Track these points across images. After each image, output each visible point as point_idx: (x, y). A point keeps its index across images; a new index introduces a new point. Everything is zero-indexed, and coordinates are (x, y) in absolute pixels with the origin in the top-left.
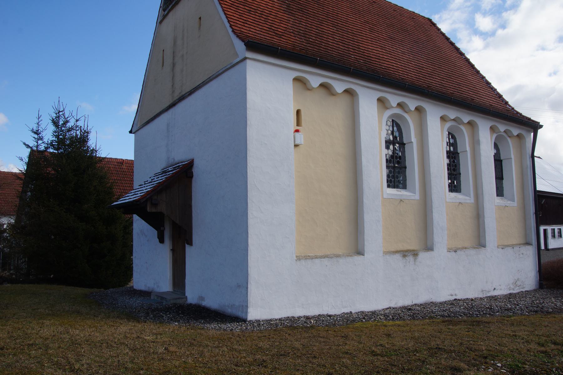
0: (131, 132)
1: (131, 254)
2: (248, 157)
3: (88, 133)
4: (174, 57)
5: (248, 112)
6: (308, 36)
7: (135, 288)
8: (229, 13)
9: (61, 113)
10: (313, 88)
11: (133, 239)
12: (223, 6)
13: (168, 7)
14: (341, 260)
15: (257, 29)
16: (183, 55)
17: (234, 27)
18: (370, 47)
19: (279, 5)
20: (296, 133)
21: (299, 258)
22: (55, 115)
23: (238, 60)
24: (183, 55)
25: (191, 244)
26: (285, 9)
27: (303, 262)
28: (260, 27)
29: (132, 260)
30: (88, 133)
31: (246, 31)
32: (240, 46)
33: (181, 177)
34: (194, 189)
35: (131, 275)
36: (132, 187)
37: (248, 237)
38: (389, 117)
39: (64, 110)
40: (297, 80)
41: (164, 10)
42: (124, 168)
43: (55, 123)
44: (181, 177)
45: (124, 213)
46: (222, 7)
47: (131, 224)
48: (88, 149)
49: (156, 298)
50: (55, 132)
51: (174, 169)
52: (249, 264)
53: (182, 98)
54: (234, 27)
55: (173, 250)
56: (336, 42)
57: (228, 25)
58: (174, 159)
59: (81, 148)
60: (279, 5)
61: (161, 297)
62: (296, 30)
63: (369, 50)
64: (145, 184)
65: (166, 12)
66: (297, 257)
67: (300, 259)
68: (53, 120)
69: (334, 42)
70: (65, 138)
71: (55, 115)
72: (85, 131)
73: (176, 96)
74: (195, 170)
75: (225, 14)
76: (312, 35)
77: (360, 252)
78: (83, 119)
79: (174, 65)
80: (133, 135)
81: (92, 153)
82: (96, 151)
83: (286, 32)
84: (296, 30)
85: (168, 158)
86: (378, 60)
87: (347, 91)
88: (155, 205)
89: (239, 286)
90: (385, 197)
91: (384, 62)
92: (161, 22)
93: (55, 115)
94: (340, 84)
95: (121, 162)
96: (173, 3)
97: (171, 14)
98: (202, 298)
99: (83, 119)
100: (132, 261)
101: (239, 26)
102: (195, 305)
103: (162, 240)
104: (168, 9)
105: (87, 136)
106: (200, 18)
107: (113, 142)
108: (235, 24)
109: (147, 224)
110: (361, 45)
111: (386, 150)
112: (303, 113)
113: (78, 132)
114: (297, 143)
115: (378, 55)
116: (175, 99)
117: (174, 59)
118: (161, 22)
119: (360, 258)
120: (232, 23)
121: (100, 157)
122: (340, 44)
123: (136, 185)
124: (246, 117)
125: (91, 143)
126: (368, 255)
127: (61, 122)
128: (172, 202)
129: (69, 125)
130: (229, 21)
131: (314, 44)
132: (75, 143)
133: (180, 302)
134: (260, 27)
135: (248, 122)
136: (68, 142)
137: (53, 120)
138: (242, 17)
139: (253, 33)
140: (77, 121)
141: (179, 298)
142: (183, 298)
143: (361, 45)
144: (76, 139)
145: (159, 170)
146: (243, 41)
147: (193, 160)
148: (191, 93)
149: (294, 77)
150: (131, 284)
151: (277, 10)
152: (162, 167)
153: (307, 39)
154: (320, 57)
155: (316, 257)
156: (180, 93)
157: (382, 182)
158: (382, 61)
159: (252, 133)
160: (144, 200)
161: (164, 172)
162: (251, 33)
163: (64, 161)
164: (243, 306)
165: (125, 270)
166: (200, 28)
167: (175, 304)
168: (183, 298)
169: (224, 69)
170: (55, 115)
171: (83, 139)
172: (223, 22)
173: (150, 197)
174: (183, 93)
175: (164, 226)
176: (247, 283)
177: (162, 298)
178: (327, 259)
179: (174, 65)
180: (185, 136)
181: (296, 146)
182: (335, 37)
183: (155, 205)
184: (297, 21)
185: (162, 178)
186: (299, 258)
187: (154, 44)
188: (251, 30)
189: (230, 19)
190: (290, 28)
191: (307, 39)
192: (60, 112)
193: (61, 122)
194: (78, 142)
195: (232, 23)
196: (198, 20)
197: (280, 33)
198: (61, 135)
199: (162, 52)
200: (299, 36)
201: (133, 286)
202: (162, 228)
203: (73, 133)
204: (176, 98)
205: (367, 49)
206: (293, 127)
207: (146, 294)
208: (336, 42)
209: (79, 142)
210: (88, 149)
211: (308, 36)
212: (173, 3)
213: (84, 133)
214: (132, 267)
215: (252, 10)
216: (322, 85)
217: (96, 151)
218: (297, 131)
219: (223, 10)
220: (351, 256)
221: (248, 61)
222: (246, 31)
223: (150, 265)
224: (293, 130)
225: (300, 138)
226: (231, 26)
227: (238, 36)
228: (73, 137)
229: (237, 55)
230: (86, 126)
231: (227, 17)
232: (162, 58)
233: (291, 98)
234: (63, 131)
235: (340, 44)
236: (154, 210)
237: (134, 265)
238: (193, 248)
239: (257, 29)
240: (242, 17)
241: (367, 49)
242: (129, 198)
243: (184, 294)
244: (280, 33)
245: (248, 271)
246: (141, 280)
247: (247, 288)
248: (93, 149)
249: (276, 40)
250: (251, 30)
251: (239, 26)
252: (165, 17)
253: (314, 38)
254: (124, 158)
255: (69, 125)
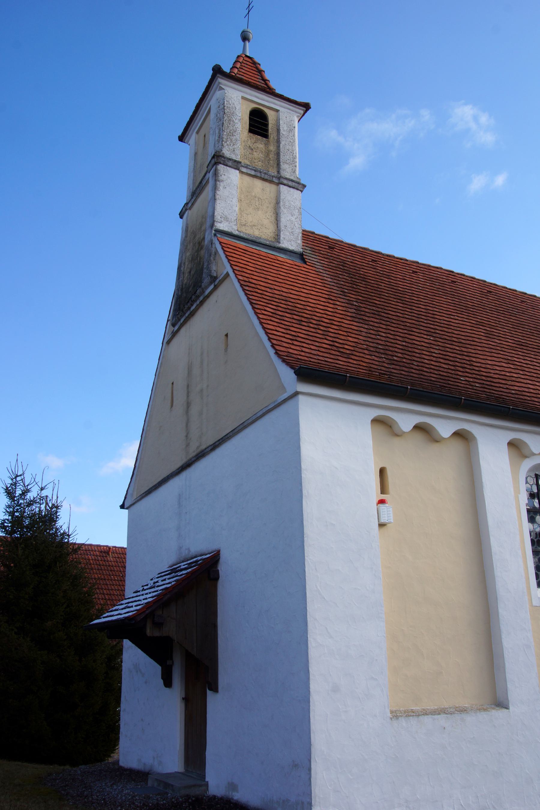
0: (122, 507)
1: (118, 702)
2: (306, 547)
3: (57, 507)
4: (188, 393)
5: (303, 475)
6: (390, 353)
7: (121, 764)
8: (269, 327)
9: (19, 479)
10: (404, 433)
11: (121, 678)
12: (261, 316)
13: (179, 320)
14: (470, 719)
15: (313, 347)
16: (202, 390)
17: (277, 347)
18: (490, 362)
19: (344, 309)
20: (381, 505)
21: (395, 715)
22: (10, 482)
23: (285, 396)
24: (202, 390)
25: (215, 689)
26: (354, 315)
27: (403, 722)
28: (317, 344)
29: (118, 714)
30: (57, 507)
31: (296, 352)
32: (287, 375)
33: (200, 579)
34: (219, 598)
35: (117, 740)
36: (124, 595)
37: (308, 679)
38: (530, 470)
39: (23, 474)
40: (377, 421)
41: (174, 325)
42: (109, 562)
43: (10, 493)
44: (200, 579)
45: (109, 637)
46: (259, 318)
47: (120, 652)
48: (56, 532)
49: (156, 784)
50: (9, 507)
51: (190, 566)
52: (313, 727)
53: (201, 455)
54: (277, 347)
55: (186, 700)
56: (434, 359)
57: (268, 344)
58: (189, 549)
59: (46, 531)
60: (344, 309)
61: (165, 781)
62: (371, 344)
63: (488, 366)
64: (144, 590)
65: (176, 328)
66: (392, 712)
67: (397, 717)
68: (7, 488)
69: (432, 358)
70: (22, 516)
71: (10, 482)
72: (53, 505)
73: (193, 452)
74: (222, 568)
75: (264, 328)
76: (396, 350)
77: (501, 703)
78: (50, 486)
79: (188, 405)
80: (126, 512)
81: (62, 539)
82: (69, 536)
83: (356, 349)
84: (371, 344)
85: (180, 548)
86: (503, 382)
87: (459, 435)
88: (158, 625)
89: (295, 766)
90: (535, 603)
91: (513, 383)
92: (169, 342)
93: (10, 482)
94: (445, 424)
95: (105, 551)
96: (187, 315)
97: (183, 330)
98: (233, 786)
99: (50, 486)
100: (119, 715)
101: (285, 345)
102: (222, 798)
103: (168, 682)
104: (179, 324)
105: (56, 512)
106: (227, 335)
107: (94, 519)
108: (279, 343)
109: (145, 655)
110: (474, 359)
111: (530, 524)
112: (389, 473)
113: (43, 507)
114: (382, 521)
115: (503, 373)
116: (191, 456)
117: (188, 396)
118: (169, 342)
119: (500, 713)
120: (275, 342)
121: (75, 544)
122: (442, 361)
123: (129, 593)
124: (301, 484)
125: (63, 523)
126: (516, 708)
127: (18, 492)
128: (185, 621)
129: (30, 496)
130: (269, 339)
131: (401, 364)
132: (38, 523)
133: (197, 792)
134: (317, 344)
135: (305, 492)
136: (27, 522)
137: (7, 488)
138: (289, 332)
139: (307, 355)
140: (42, 489)
141: (194, 786)
142: (200, 786)
143: (474, 359)
144: (39, 518)
145: (165, 567)
146: (292, 367)
147: (218, 552)
148: (215, 446)
149: (372, 418)
150: (115, 756)
151: (341, 316)
152: (171, 563)
153: (390, 357)
154: (412, 384)
155: (425, 713)
156: (198, 447)
157: (527, 579)
158: (509, 383)
159: (311, 508)
160: (143, 616)
161: (174, 571)
162: (303, 354)
163: (20, 552)
164: (303, 803)
165: (106, 731)
166: (226, 350)
167: (188, 796)
168: (200, 786)
169: (264, 411)
170: (10, 482)
171: (50, 518)
172: (261, 340)
173: (152, 612)
174: (203, 447)
175: (172, 659)
176: (310, 761)
177: (167, 785)
178: (443, 716)
179: (188, 405)
180: (206, 515)
181: (381, 525)
182: (432, 350)
183: (158, 625)
184: (372, 332)
185: (169, 582)
186: (395, 715)
187: (158, 374)
188: (304, 349)
189: (271, 336)
190: (362, 342)
191: (390, 357)
192: (17, 476)
193: (18, 492)
194: (42, 522)
195: (275, 342)
196: (224, 337)
197: (348, 352)
198: (17, 511)
199: (170, 385)
200: (377, 354)
201: (118, 762)
202: (169, 662)
203: (35, 508)
204: (192, 453)
205: (484, 366)
206: (375, 494)
207: (139, 776)
208: (434, 359)
209: (44, 522)
210: (56, 532)
211: (390, 353)
212: (187, 315)
213: (51, 508)
214: (119, 726)
215: (303, 319)
216: (418, 428)
217: (69, 536)
218: (382, 502)
219: (261, 323)
220: (485, 710)
221: (301, 397)
222: (296, 352)
223: (148, 726)
224: (375, 501)
225: (388, 513)
226: (273, 346)
227: (284, 361)
228: (34, 515)
229: (283, 389)
230: (55, 497)
231: (267, 333)
232: (170, 395)
233: (370, 450)
234: (20, 505)
235: (442, 361)
236: (157, 634)
237: (122, 723)
238: (219, 696)
239: (313, 347)
240: (289, 332)
241: (484, 366)
242: (119, 613)
243: (203, 777)
244: (348, 352)
245: (310, 738)
246: (131, 752)
247: (310, 769)
248: (64, 533)
249: (341, 362)
250: (304, 349)
251: (285, 345)
252: (174, 334)
253: (399, 355)
254: (111, 544)
255: (30, 496)
